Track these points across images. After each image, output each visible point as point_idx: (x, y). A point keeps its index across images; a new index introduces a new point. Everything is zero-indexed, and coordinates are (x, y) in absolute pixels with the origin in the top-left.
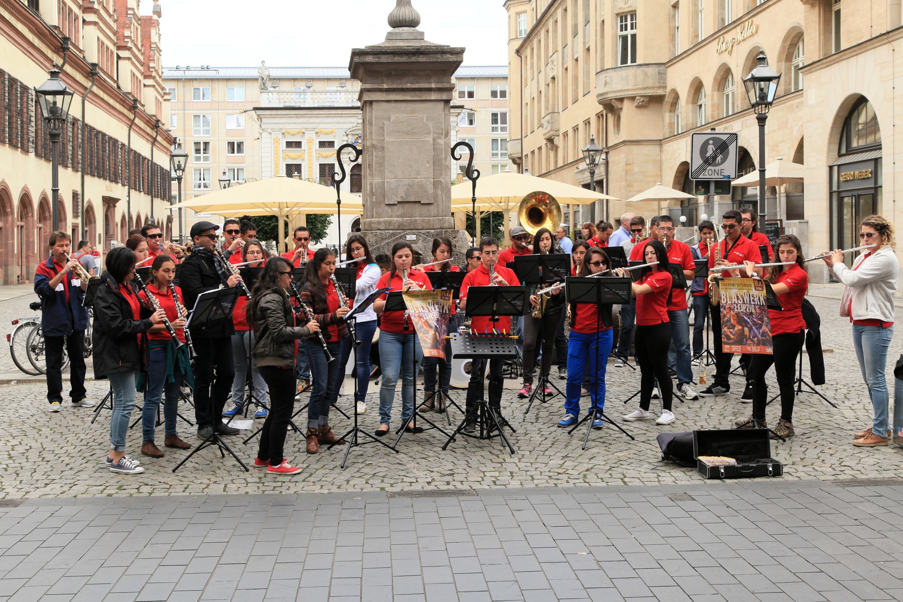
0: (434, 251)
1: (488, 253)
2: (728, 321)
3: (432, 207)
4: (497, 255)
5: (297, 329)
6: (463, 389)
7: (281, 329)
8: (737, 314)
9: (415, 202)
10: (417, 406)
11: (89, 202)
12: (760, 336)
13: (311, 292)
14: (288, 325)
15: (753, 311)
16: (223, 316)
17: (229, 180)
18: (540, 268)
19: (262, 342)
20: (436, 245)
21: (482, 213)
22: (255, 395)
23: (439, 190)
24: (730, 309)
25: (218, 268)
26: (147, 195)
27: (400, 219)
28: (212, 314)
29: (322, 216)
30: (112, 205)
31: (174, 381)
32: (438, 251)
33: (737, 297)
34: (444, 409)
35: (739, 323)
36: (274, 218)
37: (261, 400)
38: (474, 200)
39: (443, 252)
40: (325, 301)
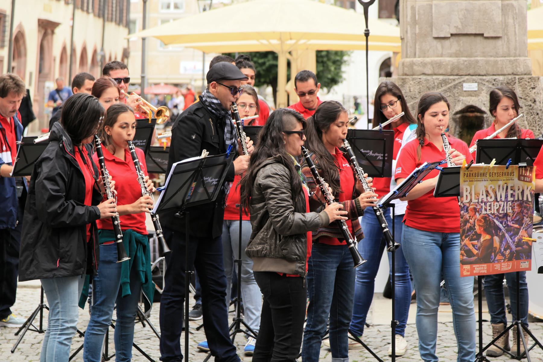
2: (472, 228)
3: (499, 43)
5: (310, 216)
7: (287, 217)
8: (485, 218)
9: (476, 35)
10: (484, 346)
11: (20, 26)
12: (513, 247)
14: (296, 210)
15: (510, 211)
16: (205, 197)
19: (261, 235)
22: (245, 320)
24: (475, 210)
26: (97, 19)
27: (454, 60)
28: (190, 193)
29: (336, 53)
30: (49, 31)
31: (129, 292)
32: (499, 109)
33: (487, 192)
34: (525, 353)
35: (487, 231)
36: (273, 55)
39: (507, 109)
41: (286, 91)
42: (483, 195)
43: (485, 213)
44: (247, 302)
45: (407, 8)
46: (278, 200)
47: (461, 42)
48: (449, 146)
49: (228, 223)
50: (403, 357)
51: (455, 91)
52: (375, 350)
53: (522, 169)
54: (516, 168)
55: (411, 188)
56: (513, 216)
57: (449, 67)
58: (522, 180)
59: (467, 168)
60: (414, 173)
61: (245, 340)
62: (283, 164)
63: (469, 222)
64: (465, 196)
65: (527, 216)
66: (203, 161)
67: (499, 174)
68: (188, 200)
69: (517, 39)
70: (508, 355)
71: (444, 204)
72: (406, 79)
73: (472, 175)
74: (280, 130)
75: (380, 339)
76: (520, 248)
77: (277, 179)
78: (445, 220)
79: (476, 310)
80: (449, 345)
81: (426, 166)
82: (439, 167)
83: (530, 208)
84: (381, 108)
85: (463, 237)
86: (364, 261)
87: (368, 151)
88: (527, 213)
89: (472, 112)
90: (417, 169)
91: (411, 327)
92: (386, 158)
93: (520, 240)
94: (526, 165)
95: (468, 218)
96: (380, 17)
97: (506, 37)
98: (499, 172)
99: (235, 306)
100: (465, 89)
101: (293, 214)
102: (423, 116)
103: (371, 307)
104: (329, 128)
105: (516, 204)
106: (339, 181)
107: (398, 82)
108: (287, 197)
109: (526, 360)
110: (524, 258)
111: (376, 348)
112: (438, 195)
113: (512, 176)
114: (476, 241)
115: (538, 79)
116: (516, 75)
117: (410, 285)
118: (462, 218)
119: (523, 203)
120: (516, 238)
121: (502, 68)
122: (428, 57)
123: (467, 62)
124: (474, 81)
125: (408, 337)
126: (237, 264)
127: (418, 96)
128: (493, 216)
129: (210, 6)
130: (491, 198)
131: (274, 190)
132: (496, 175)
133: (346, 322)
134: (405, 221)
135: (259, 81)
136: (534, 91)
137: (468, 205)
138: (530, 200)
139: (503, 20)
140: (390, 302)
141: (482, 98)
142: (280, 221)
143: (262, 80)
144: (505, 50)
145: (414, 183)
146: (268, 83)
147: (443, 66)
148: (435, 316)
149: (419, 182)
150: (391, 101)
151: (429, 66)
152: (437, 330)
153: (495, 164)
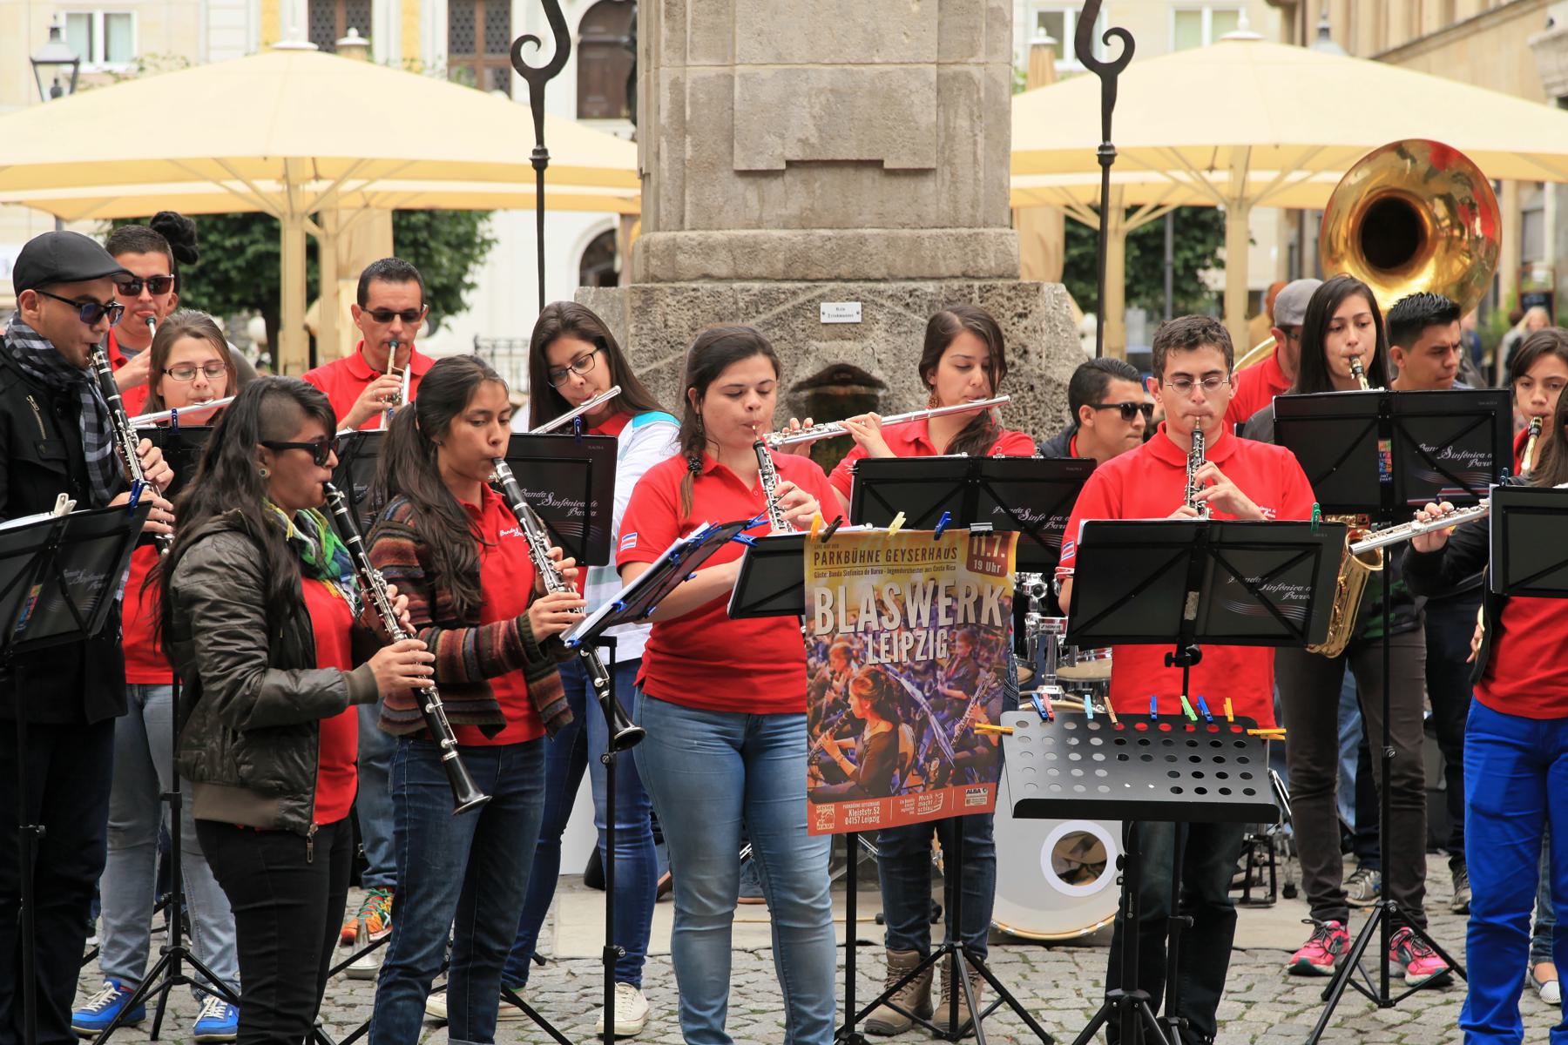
0: (928, 368)
1: (1186, 380)
2: (840, 704)
3: (928, 186)
4: (1226, 391)
6: (1236, 949)
7: (238, 683)
8: (876, 675)
10: (859, 1008)
12: (949, 751)
13: (417, 537)
15: (942, 654)
16: (70, 625)
17: (76, 63)
18: (1385, 446)
20: (937, 340)
21: (1131, 211)
22: (193, 951)
23: (963, 111)
24: (847, 654)
25: (90, 438)
27: (795, 235)
28: (25, 614)
29: (457, 216)
32: (945, 366)
33: (880, 603)
34: (970, 1024)
35: (881, 711)
36: (262, 224)
37: (215, 971)
38: (1106, 159)
40: (471, 577)
41: (307, 328)
42: (868, 612)
43: (876, 660)
44: (198, 906)
45: (658, 85)
46: (219, 635)
47: (817, 185)
48: (775, 475)
49: (137, 694)
50: (636, 1041)
51: (797, 324)
52: (561, 1023)
53: (980, 541)
54: (963, 538)
55: (662, 593)
56: (950, 666)
57: (780, 256)
58: (977, 571)
59: (825, 538)
60: (672, 554)
61: (197, 1005)
62: (246, 534)
63: (831, 688)
64: (818, 618)
65: (988, 666)
66: (60, 524)
67: (913, 554)
68: (20, 634)
69: (981, 175)
70: (925, 1029)
71: (757, 638)
72: (654, 290)
73: (839, 557)
74: (246, 441)
75: (575, 996)
76: (966, 753)
77: (221, 577)
78: (757, 681)
79: (841, 915)
80: (764, 1006)
81: (704, 533)
82: (742, 536)
83: (997, 645)
84: (551, 379)
85: (817, 730)
86: (481, 797)
87: (543, 494)
88: (988, 660)
89: (845, 383)
90: (680, 541)
91: (661, 962)
92: (593, 514)
93: (966, 732)
94: (991, 528)
95: (829, 676)
96: (581, 115)
97: (947, 169)
98: (914, 548)
99: (167, 915)
100: (824, 319)
101: (265, 672)
102: (702, 395)
103: (549, 911)
104: (447, 429)
105: (959, 633)
106: (477, 575)
107: (632, 300)
108: (249, 626)
109: (974, 1040)
110: (977, 780)
111: (563, 1019)
112: (740, 611)
113: (950, 559)
114: (852, 739)
115: (1038, 289)
116: (973, 278)
117: (652, 854)
118: (812, 677)
119: (978, 633)
120: (957, 727)
121: (933, 258)
122: (719, 229)
123: (834, 241)
124: (852, 297)
125: (651, 987)
126: (166, 805)
127: (687, 339)
128: (897, 670)
129: (74, 81)
130: (891, 620)
131: (210, 609)
132: (907, 556)
133: (497, 947)
134: (641, 684)
135: (228, 301)
136: (1024, 323)
137: (827, 640)
138: (998, 622)
139: (942, 119)
140: (599, 900)
141: (874, 345)
142: (220, 691)
143: (235, 297)
144: (945, 206)
145: (673, 582)
146: (253, 306)
147: (762, 253)
148: (727, 933)
149: (686, 578)
150: (577, 355)
151: (723, 254)
152: (730, 969)
153: (904, 526)
